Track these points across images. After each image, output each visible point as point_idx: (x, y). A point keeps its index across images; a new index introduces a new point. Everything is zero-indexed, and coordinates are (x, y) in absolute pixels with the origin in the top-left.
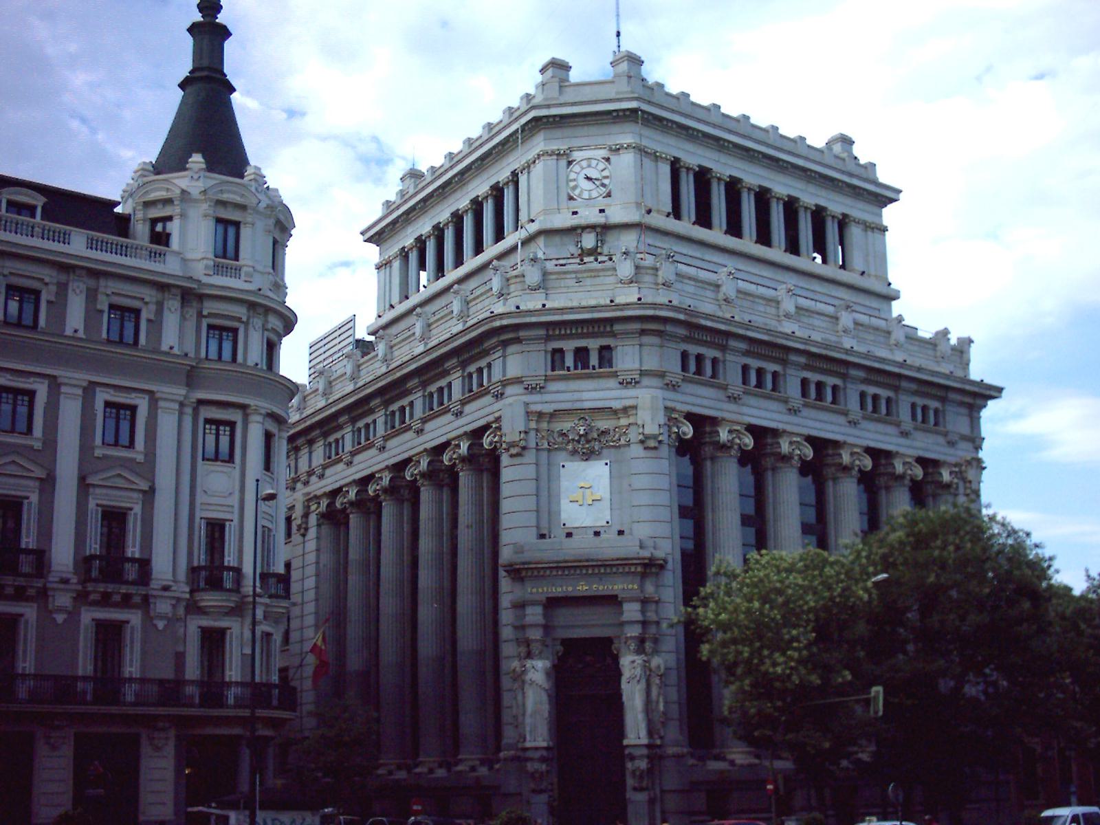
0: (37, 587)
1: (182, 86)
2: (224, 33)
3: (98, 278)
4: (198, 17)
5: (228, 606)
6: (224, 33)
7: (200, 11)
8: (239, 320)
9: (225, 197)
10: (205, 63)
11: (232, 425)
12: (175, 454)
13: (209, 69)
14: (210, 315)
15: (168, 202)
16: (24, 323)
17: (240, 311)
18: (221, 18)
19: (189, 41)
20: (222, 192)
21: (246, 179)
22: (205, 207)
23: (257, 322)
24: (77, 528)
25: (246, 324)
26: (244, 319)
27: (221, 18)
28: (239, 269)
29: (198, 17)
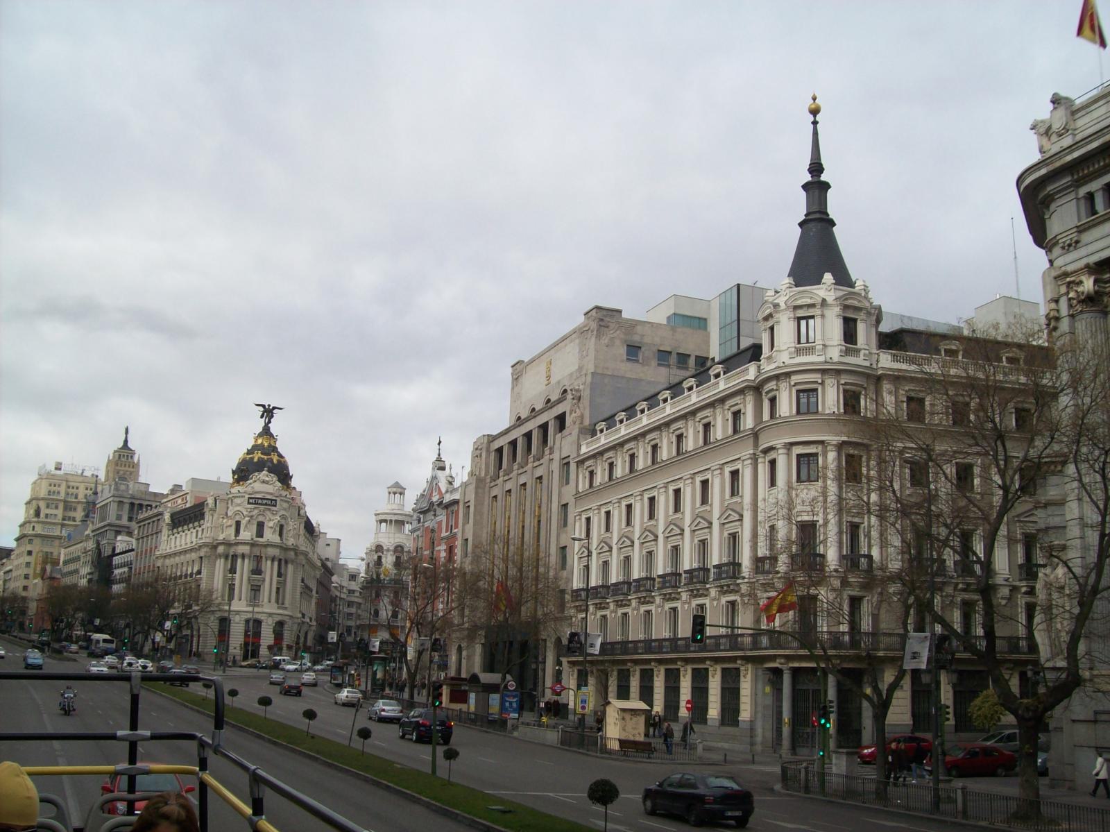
0: (600, 721)
1: (801, 225)
2: (826, 186)
3: (840, 374)
4: (808, 178)
5: (483, 825)
6: (826, 186)
7: (810, 173)
8: (816, 382)
9: (799, 303)
10: (815, 208)
11: (816, 455)
12: (21, 742)
13: (820, 212)
14: (796, 384)
15: (813, 306)
16: (811, 411)
17: (816, 377)
18: (823, 178)
19: (804, 194)
20: (847, 299)
21: (857, 288)
22: (837, 310)
23: (783, 385)
24: (283, 796)
25: (822, 383)
26: (820, 381)
27: (823, 178)
28: (813, 348)
29: (808, 178)
